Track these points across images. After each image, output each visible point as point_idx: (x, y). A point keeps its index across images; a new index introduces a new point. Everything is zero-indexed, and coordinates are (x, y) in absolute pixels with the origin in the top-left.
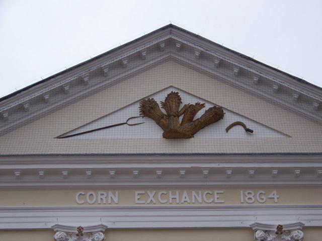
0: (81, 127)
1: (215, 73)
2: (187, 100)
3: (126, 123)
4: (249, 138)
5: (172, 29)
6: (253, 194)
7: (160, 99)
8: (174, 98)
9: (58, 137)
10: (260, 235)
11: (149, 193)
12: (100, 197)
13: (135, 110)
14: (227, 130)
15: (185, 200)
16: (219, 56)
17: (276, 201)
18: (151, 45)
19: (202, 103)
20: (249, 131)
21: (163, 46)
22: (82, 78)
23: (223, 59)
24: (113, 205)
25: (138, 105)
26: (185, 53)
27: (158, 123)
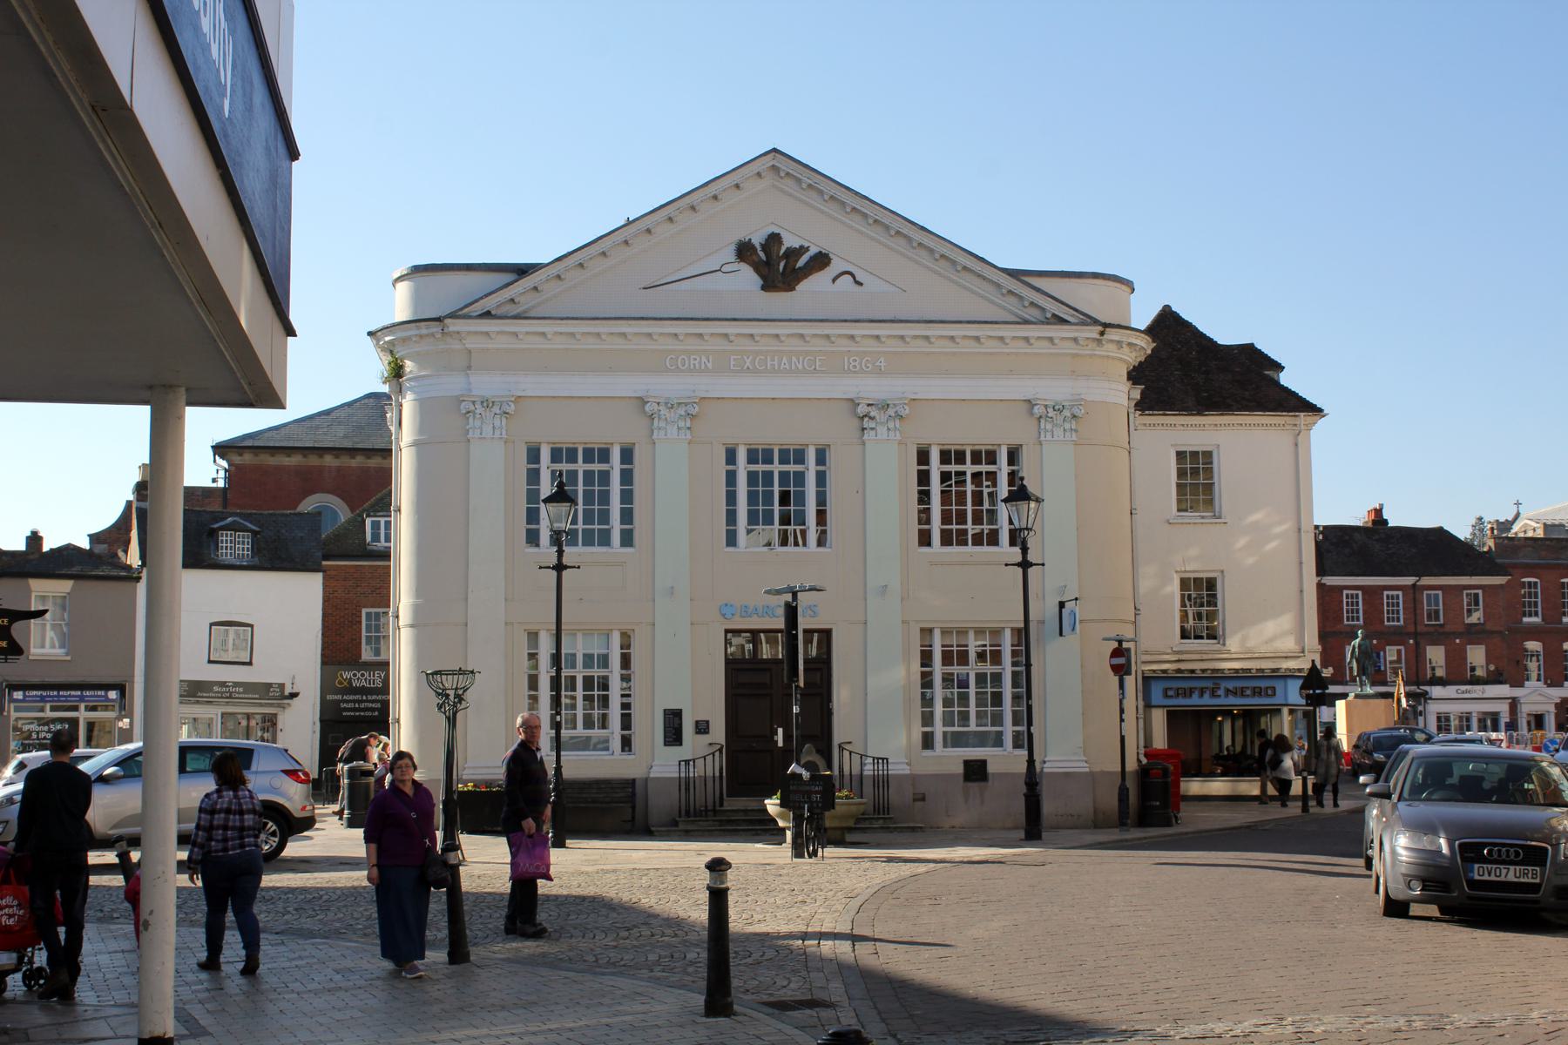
2: (790, 242)
7: (757, 240)
8: (774, 239)
9: (644, 288)
13: (732, 257)
14: (834, 280)
21: (558, 718)
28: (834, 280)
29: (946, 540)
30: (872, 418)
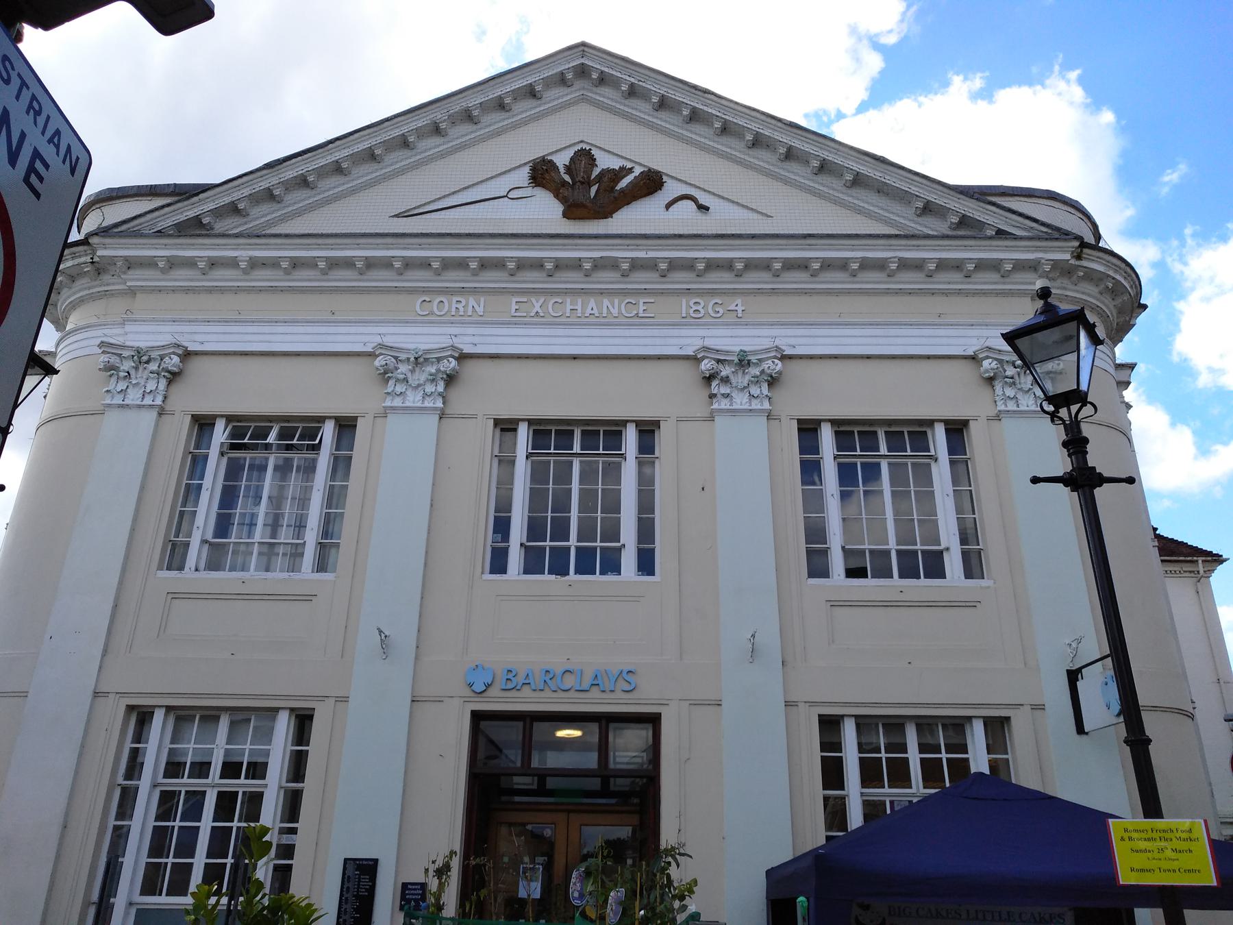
0: (429, 203)
1: (747, 158)
2: (605, 162)
3: (506, 196)
4: (708, 218)
5: (586, 49)
6: (702, 304)
7: (562, 160)
8: (584, 157)
9: (397, 216)
10: (709, 365)
11: (533, 300)
12: (454, 305)
13: (523, 176)
14: (668, 206)
15: (592, 312)
16: (659, 89)
17: (740, 315)
18: (550, 74)
19: (629, 165)
20: (703, 208)
21: (570, 76)
22: (436, 123)
23: (665, 93)
24: (475, 318)
25: (527, 169)
26: (761, 153)
27: (557, 196)
28: (668, 206)
29: (533, 564)
30: (726, 380)
